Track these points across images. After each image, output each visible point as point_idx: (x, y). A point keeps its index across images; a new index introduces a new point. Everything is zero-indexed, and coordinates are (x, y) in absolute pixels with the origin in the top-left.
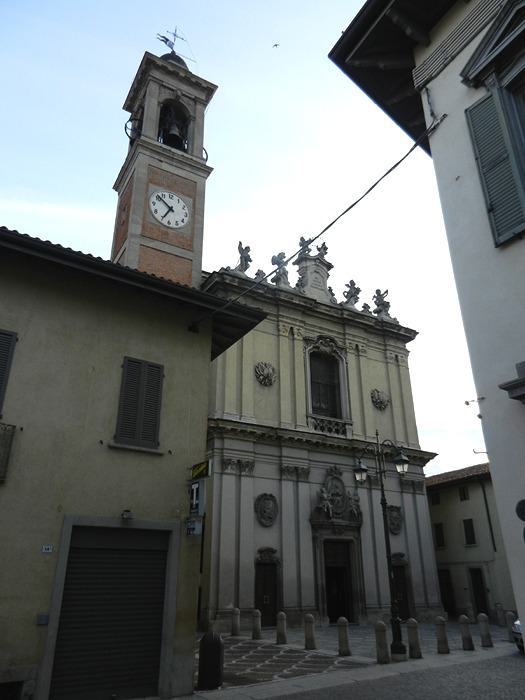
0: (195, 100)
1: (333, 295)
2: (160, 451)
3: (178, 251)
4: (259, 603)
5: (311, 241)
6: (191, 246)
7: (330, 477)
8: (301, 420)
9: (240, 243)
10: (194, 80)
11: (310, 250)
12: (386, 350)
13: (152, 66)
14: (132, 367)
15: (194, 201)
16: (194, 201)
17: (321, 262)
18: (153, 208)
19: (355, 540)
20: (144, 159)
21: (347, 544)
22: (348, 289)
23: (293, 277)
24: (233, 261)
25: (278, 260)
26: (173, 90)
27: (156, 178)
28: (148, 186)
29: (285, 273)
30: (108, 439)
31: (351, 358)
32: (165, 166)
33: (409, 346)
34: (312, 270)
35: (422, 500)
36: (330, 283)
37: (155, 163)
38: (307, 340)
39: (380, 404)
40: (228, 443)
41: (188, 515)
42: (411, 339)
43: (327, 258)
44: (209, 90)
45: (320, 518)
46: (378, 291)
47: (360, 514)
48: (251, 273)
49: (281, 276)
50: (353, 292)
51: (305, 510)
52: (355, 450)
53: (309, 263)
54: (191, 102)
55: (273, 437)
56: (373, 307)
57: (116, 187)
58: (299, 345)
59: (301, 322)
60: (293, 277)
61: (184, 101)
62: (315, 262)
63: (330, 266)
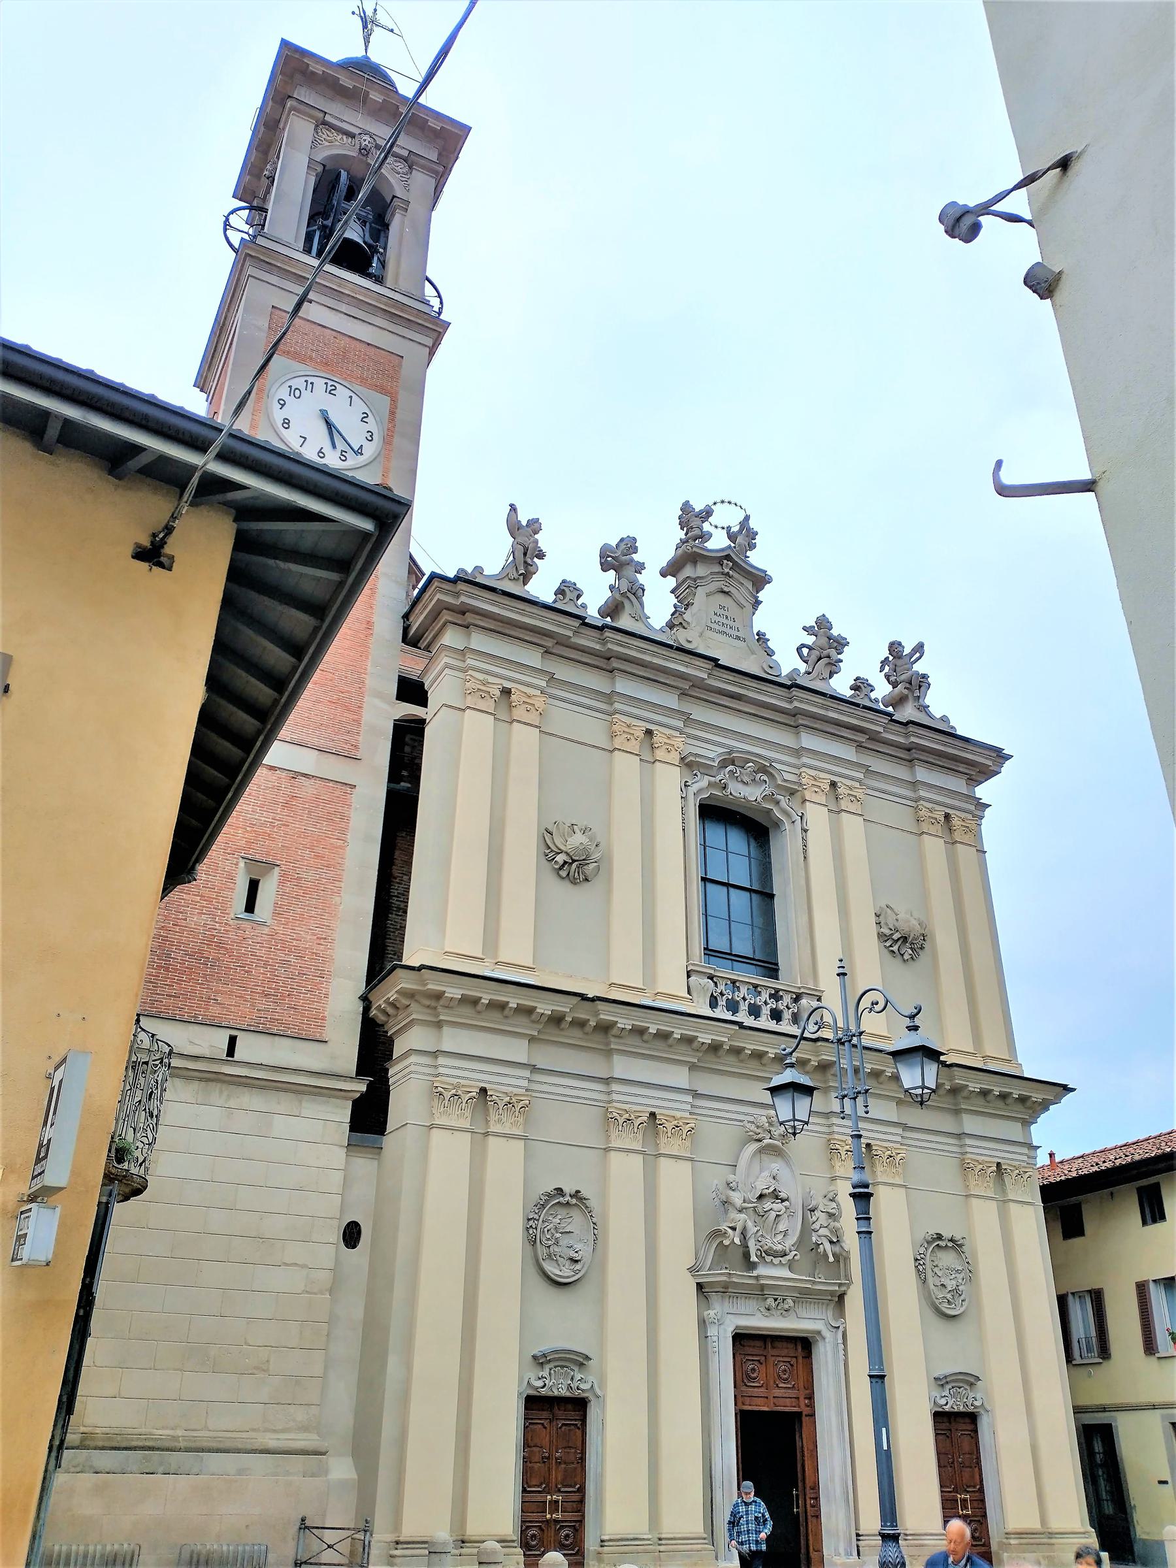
1: (770, 653)
3: (369, 546)
5: (707, 513)
7: (754, 1146)
9: (513, 508)
13: (298, 76)
15: (394, 401)
16: (394, 401)
17: (736, 566)
19: (827, 1333)
20: (270, 294)
21: (804, 1345)
24: (491, 556)
25: (619, 559)
26: (353, 136)
29: (636, 592)
31: (817, 816)
33: (983, 791)
35: (1030, 1221)
36: (761, 621)
38: (689, 764)
40: (452, 1040)
42: (987, 773)
43: (756, 558)
45: (727, 1266)
46: (895, 648)
49: (627, 596)
50: (826, 646)
51: (679, 1247)
53: (701, 570)
55: (584, 1022)
56: (882, 689)
58: (669, 778)
59: (859, 781)
60: (658, 603)
62: (720, 565)
63: (760, 580)
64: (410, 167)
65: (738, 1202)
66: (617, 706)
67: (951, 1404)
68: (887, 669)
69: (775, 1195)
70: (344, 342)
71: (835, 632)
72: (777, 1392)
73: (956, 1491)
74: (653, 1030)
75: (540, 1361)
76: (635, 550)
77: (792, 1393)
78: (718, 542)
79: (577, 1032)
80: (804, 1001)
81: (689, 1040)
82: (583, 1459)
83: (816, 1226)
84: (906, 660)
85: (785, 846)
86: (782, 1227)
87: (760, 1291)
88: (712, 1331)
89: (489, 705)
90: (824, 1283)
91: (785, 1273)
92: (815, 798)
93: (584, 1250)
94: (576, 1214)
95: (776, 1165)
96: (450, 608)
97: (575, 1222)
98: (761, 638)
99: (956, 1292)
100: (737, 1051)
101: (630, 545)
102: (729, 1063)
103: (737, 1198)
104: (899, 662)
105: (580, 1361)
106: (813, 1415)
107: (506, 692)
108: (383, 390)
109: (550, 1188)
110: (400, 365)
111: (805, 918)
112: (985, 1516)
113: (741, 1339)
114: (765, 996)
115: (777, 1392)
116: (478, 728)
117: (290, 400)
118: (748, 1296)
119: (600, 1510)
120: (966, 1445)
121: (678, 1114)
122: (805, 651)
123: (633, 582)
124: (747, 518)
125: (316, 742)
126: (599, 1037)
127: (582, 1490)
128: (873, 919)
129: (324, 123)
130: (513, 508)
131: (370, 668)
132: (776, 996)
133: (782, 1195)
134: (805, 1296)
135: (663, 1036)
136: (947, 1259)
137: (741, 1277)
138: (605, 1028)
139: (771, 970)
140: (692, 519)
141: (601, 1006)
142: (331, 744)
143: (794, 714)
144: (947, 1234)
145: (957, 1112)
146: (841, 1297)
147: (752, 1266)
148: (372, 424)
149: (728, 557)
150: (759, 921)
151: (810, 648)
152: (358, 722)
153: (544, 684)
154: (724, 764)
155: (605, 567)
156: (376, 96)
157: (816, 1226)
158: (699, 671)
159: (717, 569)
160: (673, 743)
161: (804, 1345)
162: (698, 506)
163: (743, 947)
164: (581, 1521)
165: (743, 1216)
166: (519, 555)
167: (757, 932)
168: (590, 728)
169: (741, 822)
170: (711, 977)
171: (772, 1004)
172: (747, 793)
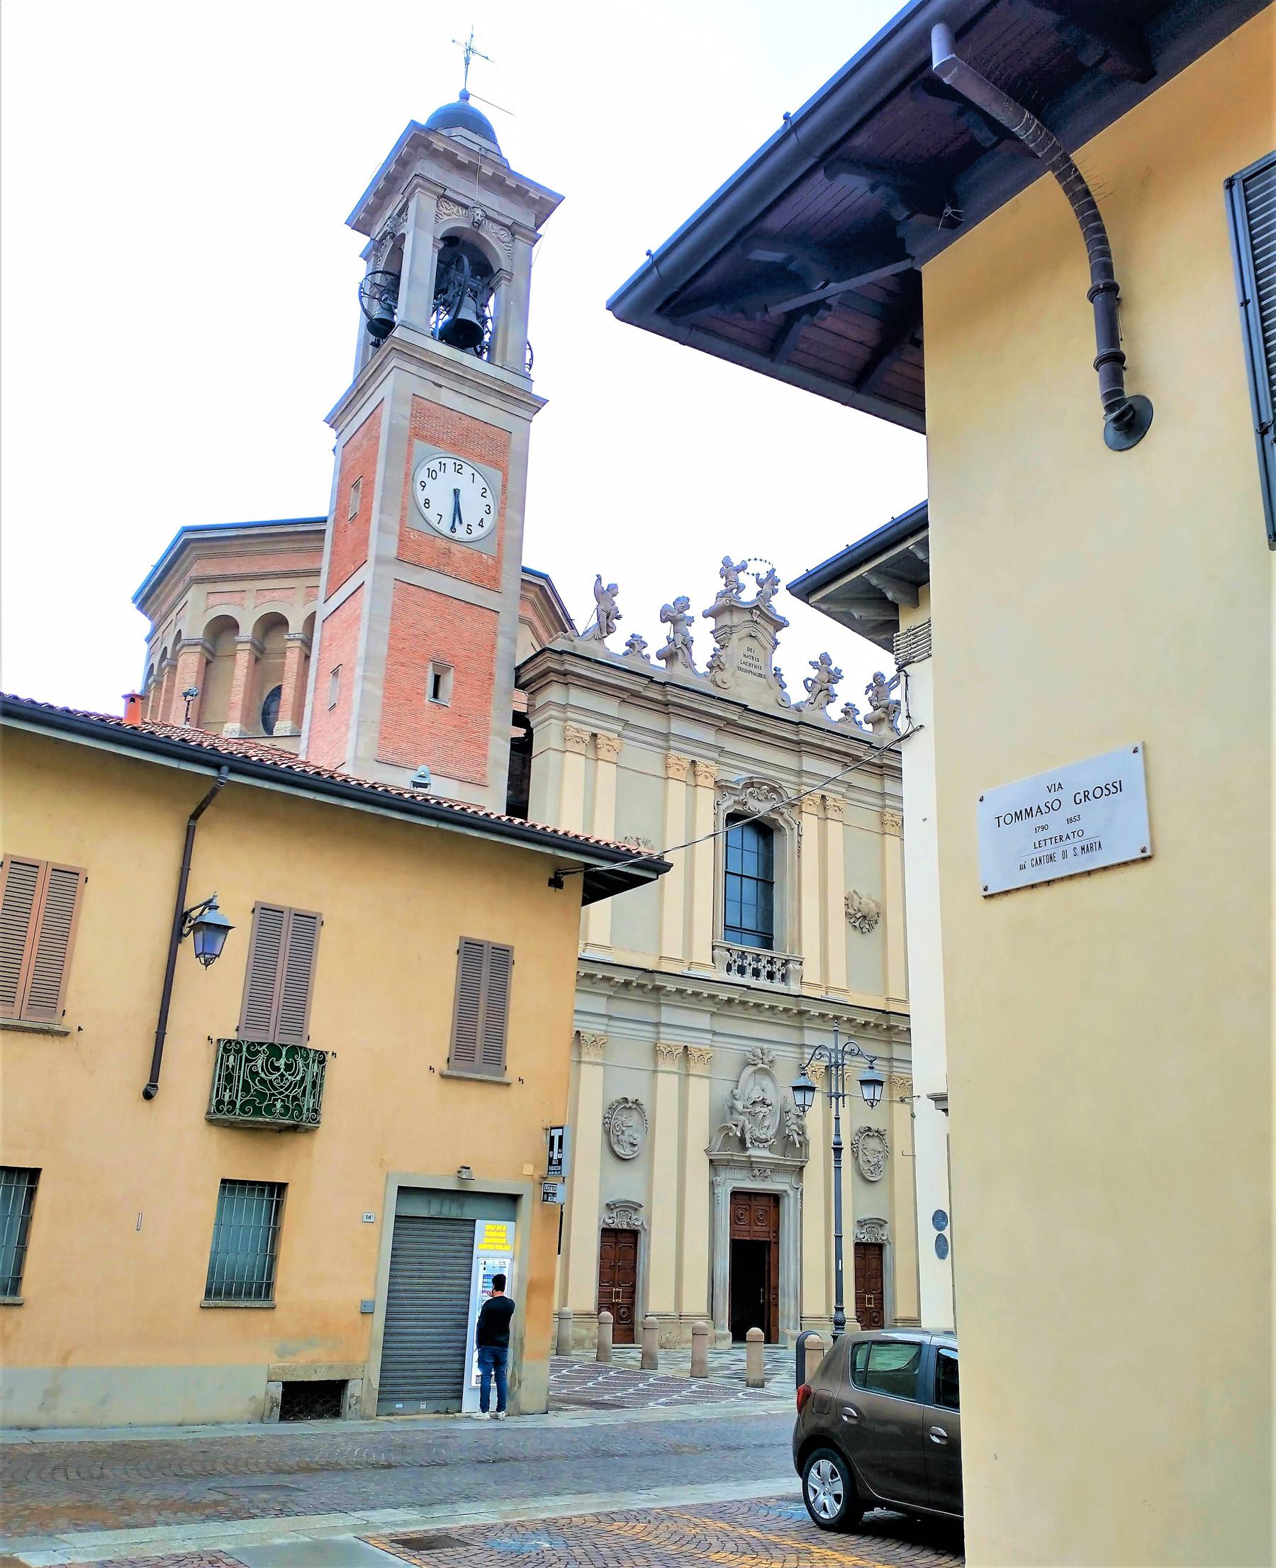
0: (513, 229)
1: (783, 686)
2: (505, 1080)
4: (605, 1301)
5: (743, 568)
6: (495, 580)
7: (750, 1069)
8: (702, 952)
9: (599, 578)
10: (511, 182)
11: (740, 588)
12: (884, 807)
14: (470, 951)
15: (505, 475)
16: (505, 475)
18: (421, 496)
19: (791, 1193)
21: (775, 1199)
22: (813, 673)
23: (703, 648)
25: (675, 615)
26: (466, 207)
27: (427, 427)
28: (410, 444)
29: (688, 643)
30: (441, 1065)
31: (809, 824)
32: (447, 398)
34: (744, 632)
36: (778, 659)
37: (426, 391)
38: (720, 786)
39: (864, 920)
41: (544, 1173)
44: (543, 204)
45: (730, 1146)
47: (804, 1144)
48: (616, 644)
50: (826, 678)
51: (699, 1134)
52: (798, 1014)
53: (736, 619)
54: (505, 235)
56: (865, 709)
57: (334, 420)
58: (706, 798)
60: (703, 648)
61: (491, 234)
64: (513, 235)
65: (740, 1108)
66: (672, 744)
67: (867, 1238)
68: (871, 692)
69: (763, 1102)
70: (466, 422)
71: (832, 668)
72: (756, 1228)
73: (865, 1292)
74: (690, 992)
75: (610, 1207)
76: (688, 607)
77: (766, 1229)
78: (749, 595)
79: (639, 992)
80: (790, 966)
81: (712, 997)
82: (635, 1267)
83: (789, 1123)
84: (886, 687)
85: (784, 847)
86: (766, 1123)
87: (750, 1165)
88: (718, 1190)
89: (581, 748)
90: (790, 1161)
91: (766, 1153)
92: (810, 809)
93: (639, 1138)
94: (635, 1114)
95: (766, 1082)
96: (555, 671)
97: (633, 1119)
98: (778, 673)
99: (877, 1165)
100: (743, 1003)
101: (683, 603)
102: (738, 1011)
103: (739, 1105)
104: (880, 689)
105: (636, 1207)
106: (777, 1243)
107: (594, 735)
108: (496, 465)
109: (619, 1097)
110: (509, 441)
111: (796, 903)
112: (882, 1308)
113: (735, 1194)
114: (764, 962)
115: (756, 1228)
116: (575, 765)
117: (429, 481)
118: (741, 1168)
119: (646, 1293)
120: (874, 1264)
121: (703, 1047)
122: (810, 683)
123: (686, 635)
124: (773, 570)
125: (462, 774)
126: (654, 995)
127: (634, 1286)
128: (843, 901)
129: (444, 196)
130: (599, 578)
131: (493, 713)
132: (771, 962)
133: (768, 1102)
134: (778, 1168)
135: (696, 994)
136: (873, 1144)
137: (739, 1156)
138: (657, 989)
139: (767, 942)
140: (730, 571)
141: (657, 976)
142: (467, 775)
143: (799, 743)
144: (874, 1127)
145: (890, 1043)
146: (802, 1168)
147: (746, 1149)
148: (489, 500)
149: (757, 607)
150: (761, 902)
151: (814, 682)
152: (485, 756)
153: (620, 729)
154: (747, 786)
155: (663, 621)
156: (487, 171)
157: (789, 1123)
158: (732, 714)
159: (748, 617)
160: (710, 770)
161: (775, 1199)
162: (736, 562)
163: (749, 923)
164: (633, 1304)
165: (742, 1117)
166: (603, 619)
167: (760, 910)
168: (649, 760)
169: (758, 833)
170: (728, 950)
171: (769, 968)
172: (760, 808)
